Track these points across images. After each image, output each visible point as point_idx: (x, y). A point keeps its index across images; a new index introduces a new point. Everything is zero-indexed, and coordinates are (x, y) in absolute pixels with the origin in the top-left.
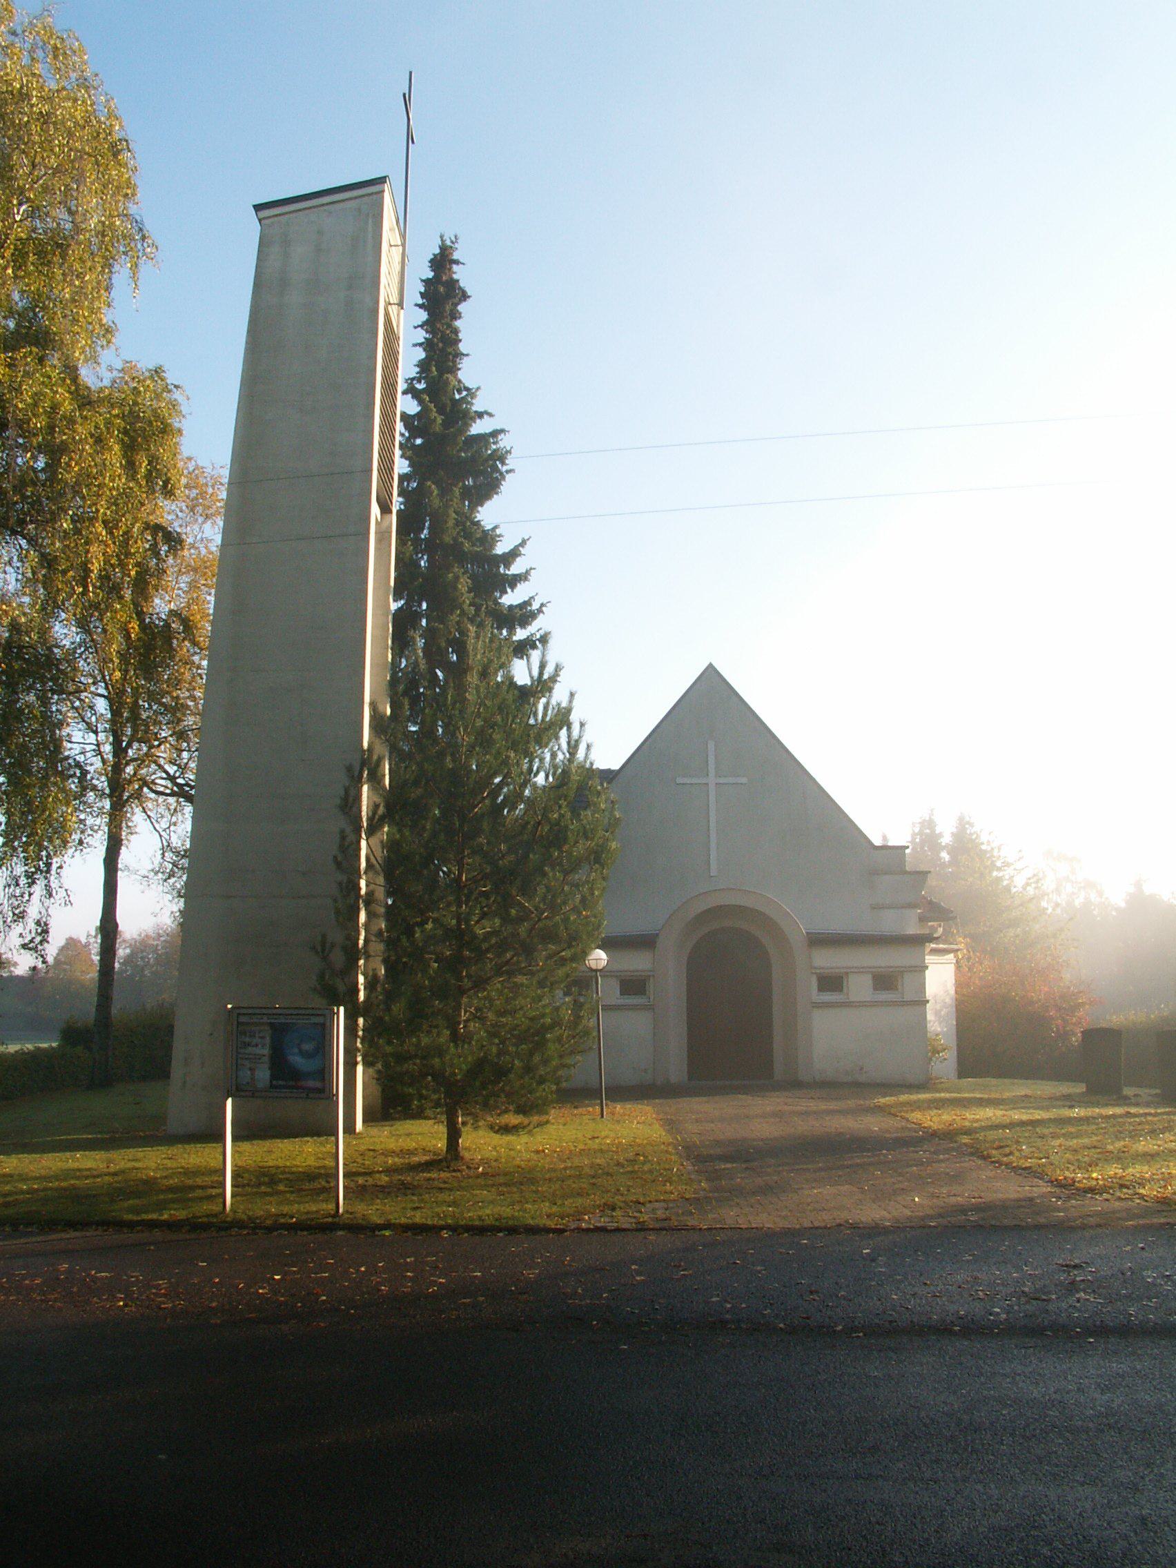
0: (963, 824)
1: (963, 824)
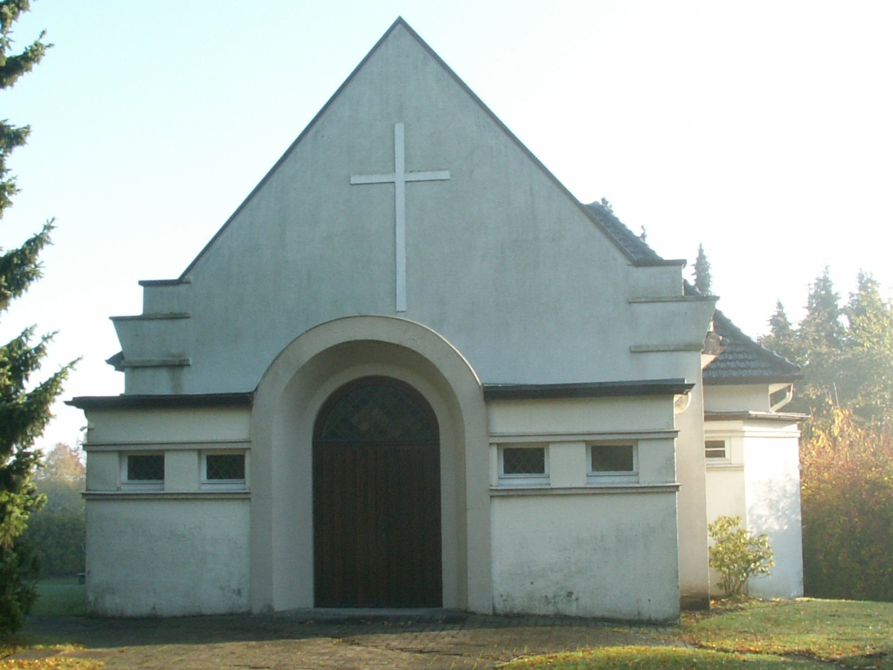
0: (865, 284)
1: (865, 284)
